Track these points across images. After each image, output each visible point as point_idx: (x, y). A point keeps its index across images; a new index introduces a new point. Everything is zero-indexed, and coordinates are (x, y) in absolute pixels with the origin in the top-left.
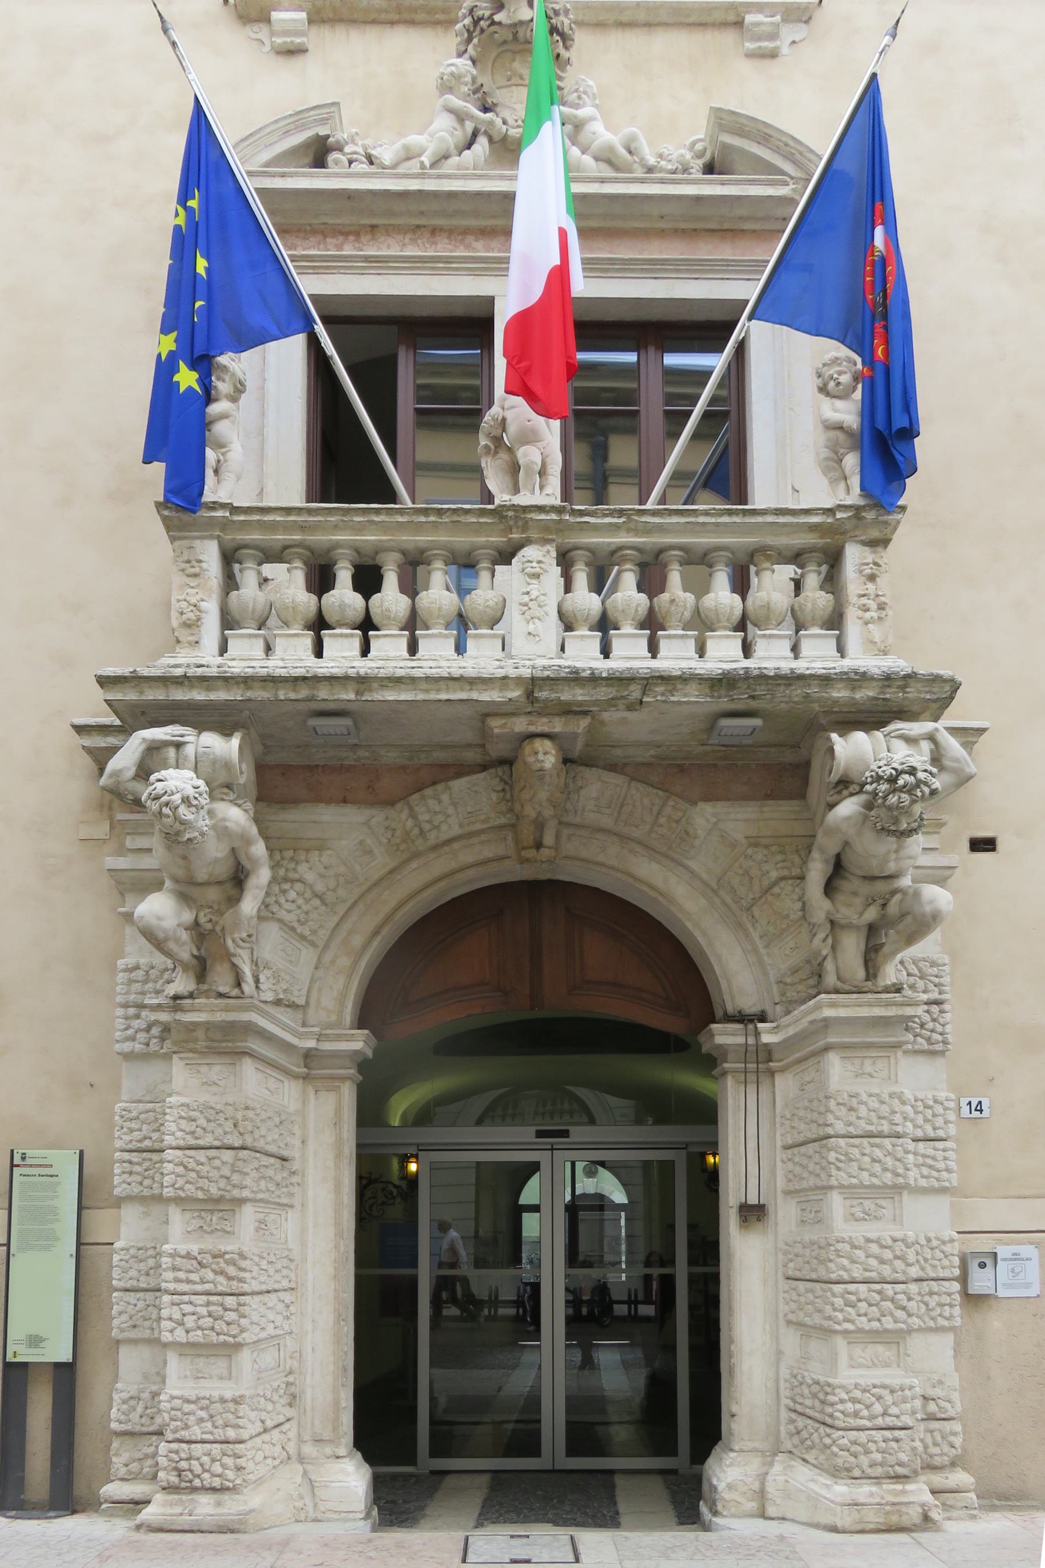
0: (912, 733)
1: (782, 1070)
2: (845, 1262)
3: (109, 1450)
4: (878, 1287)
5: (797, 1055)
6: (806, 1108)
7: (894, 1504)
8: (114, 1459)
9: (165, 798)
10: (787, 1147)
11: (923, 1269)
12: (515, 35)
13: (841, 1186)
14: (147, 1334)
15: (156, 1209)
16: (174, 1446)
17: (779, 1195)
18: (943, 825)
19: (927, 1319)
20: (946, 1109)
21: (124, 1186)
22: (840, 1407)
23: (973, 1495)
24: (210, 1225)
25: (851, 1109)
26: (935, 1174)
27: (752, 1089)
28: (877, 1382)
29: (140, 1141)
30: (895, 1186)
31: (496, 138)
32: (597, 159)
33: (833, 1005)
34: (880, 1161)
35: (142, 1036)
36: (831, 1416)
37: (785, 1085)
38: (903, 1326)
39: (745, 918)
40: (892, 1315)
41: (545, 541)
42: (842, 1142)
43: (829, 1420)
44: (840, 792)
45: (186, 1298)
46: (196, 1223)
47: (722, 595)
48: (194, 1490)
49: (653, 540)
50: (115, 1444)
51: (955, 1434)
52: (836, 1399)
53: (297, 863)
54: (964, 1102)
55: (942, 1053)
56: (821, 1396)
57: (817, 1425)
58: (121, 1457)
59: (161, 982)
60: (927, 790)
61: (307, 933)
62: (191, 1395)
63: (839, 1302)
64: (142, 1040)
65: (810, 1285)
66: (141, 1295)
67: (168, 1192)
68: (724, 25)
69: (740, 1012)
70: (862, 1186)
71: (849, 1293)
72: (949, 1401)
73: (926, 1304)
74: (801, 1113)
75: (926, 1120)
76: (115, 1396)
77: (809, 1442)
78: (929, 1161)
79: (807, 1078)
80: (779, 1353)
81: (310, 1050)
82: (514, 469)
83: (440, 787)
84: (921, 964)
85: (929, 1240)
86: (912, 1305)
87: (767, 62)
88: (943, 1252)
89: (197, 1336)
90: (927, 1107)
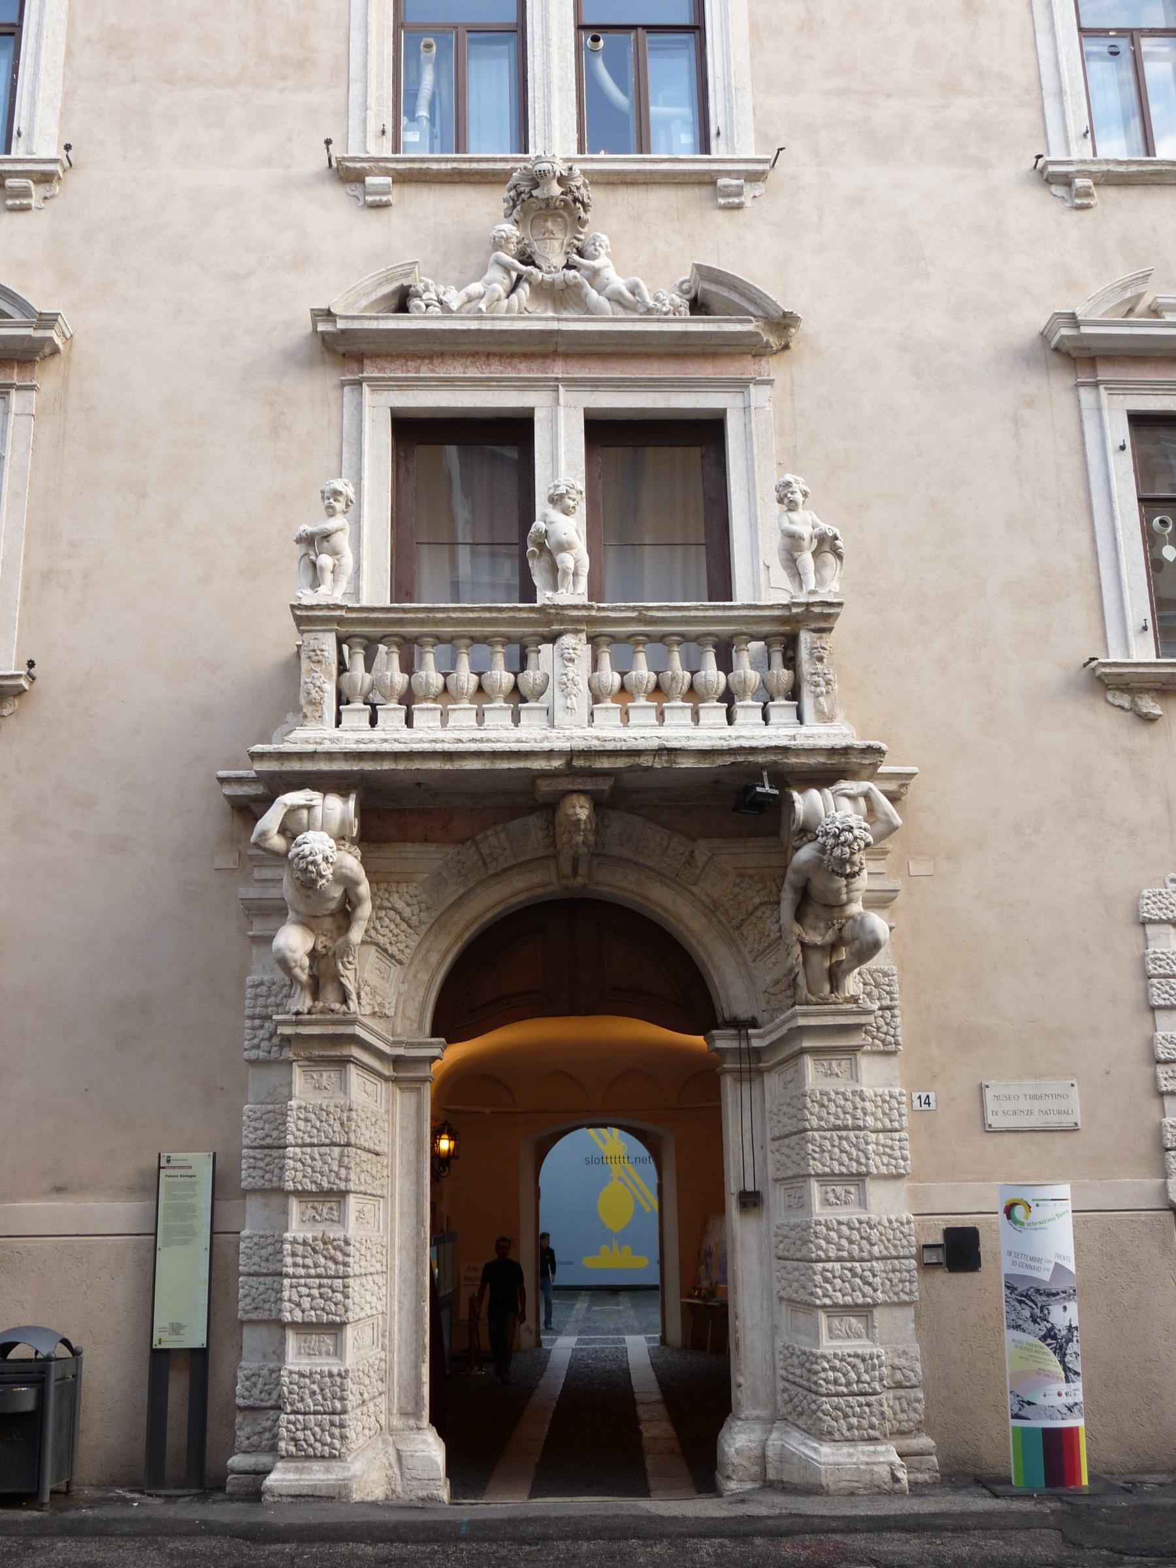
0: (852, 792)
1: (770, 1069)
2: (823, 1243)
3: (234, 1424)
4: (849, 1265)
5: (780, 1058)
6: (789, 1105)
7: (867, 1464)
8: (238, 1433)
9: (310, 858)
10: (774, 1139)
11: (886, 1248)
12: (548, 205)
13: (817, 1175)
14: (265, 1315)
15: (276, 1201)
16: (292, 1417)
17: (770, 1183)
18: (887, 853)
19: (891, 1294)
20: (899, 1103)
21: (250, 1179)
22: (823, 1375)
23: (934, 1458)
24: (320, 1215)
25: (823, 1106)
26: (893, 1162)
27: (746, 1086)
28: (851, 1352)
29: (263, 1139)
30: (859, 1174)
31: (534, 283)
32: (609, 300)
33: (805, 1015)
34: (846, 1152)
35: (265, 1044)
36: (815, 1383)
37: (772, 1082)
38: (869, 1300)
39: (736, 934)
40: (861, 1290)
41: (577, 632)
42: (816, 1135)
43: (813, 1387)
44: (801, 839)
45: (302, 1281)
46: (311, 1212)
47: (712, 674)
48: (308, 1457)
49: (658, 629)
50: (238, 1419)
51: (918, 1401)
52: (819, 1368)
53: (390, 893)
54: (915, 1095)
55: (894, 1053)
56: (807, 1365)
57: (805, 1393)
58: (244, 1430)
59: (280, 996)
60: (862, 844)
61: (396, 953)
62: (306, 1369)
63: (818, 1278)
64: (266, 1048)
65: (795, 1264)
66: (262, 1279)
67: (289, 1186)
68: (700, 183)
69: (735, 1018)
70: (833, 1174)
71: (827, 1271)
72: (912, 1370)
73: (890, 1280)
74: (785, 1108)
75: (884, 1114)
76: (240, 1374)
77: (799, 1409)
78: (888, 1151)
79: (789, 1078)
80: (775, 1328)
81: (398, 1056)
82: (554, 569)
83: (499, 827)
84: (875, 975)
85: (890, 1222)
86: (877, 1281)
87: (735, 213)
88: (902, 1232)
89: (312, 1316)
90: (884, 1101)
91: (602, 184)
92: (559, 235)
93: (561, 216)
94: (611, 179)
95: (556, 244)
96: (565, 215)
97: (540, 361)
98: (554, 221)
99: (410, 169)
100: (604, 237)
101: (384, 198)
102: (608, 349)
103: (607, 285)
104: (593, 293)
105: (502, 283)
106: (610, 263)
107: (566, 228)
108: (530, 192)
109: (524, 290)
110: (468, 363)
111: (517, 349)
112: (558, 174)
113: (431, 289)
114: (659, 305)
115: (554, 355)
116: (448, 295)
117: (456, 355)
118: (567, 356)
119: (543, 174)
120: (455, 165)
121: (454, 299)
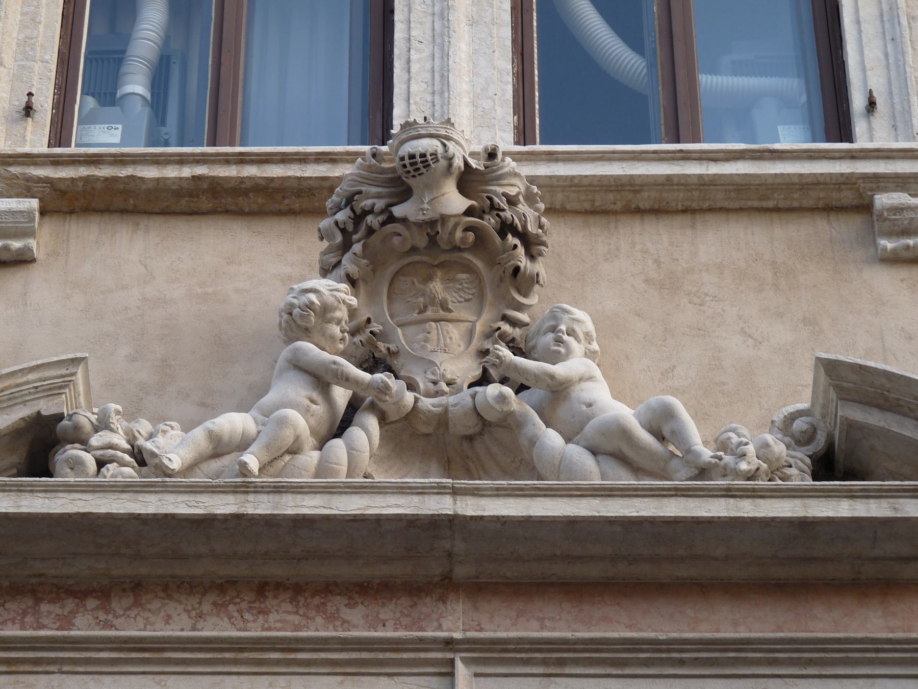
12: (433, 241)
31: (393, 417)
32: (594, 452)
68: (830, 209)
91: (577, 212)
92: (463, 312)
93: (468, 268)
94: (600, 200)
95: (455, 333)
96: (479, 264)
97: (405, 601)
98: (448, 280)
99: (87, 180)
100: (584, 319)
101: (16, 244)
102: (593, 571)
103: (589, 419)
104: (553, 438)
105: (305, 412)
106: (598, 373)
107: (481, 298)
108: (387, 209)
109: (366, 433)
110: (206, 607)
111: (345, 571)
112: (458, 163)
113: (115, 421)
114: (728, 459)
115: (445, 587)
116: (160, 439)
117: (173, 587)
118: (479, 589)
119: (419, 164)
120: (201, 170)
121: (175, 448)
